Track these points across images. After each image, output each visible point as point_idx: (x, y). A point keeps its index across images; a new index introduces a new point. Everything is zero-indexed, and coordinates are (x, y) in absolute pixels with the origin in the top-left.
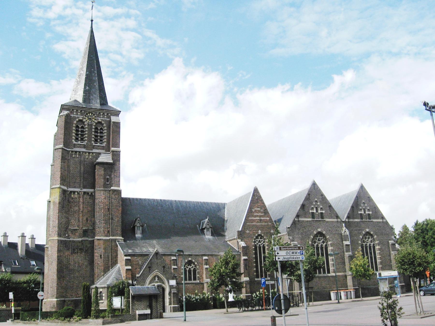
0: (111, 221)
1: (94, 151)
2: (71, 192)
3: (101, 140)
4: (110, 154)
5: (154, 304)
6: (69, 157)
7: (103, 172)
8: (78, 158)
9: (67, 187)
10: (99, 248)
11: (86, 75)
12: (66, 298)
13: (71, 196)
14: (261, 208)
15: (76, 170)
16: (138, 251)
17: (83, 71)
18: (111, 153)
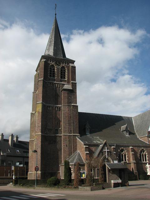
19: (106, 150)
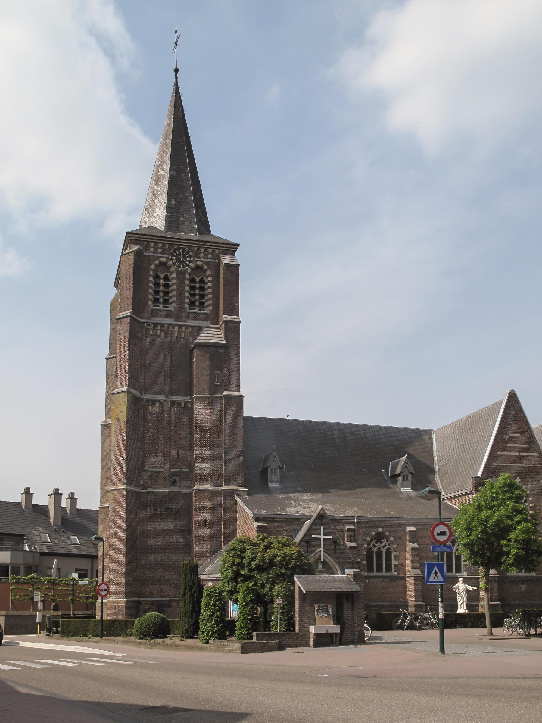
0: (223, 455)
1: (190, 323)
2: (148, 401)
3: (202, 304)
4: (218, 328)
5: (346, 613)
6: (144, 336)
7: (208, 362)
8: (159, 336)
9: (141, 393)
10: (202, 507)
11: (171, 177)
12: (141, 597)
13: (148, 409)
14: (522, 434)
15: (156, 361)
16: (277, 511)
17: (163, 170)
18: (223, 325)
19: (322, 536)
